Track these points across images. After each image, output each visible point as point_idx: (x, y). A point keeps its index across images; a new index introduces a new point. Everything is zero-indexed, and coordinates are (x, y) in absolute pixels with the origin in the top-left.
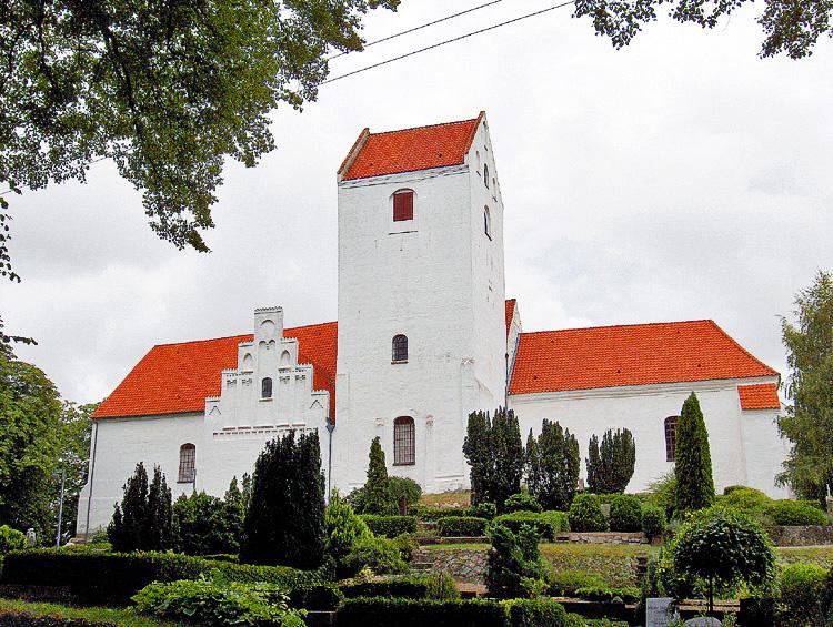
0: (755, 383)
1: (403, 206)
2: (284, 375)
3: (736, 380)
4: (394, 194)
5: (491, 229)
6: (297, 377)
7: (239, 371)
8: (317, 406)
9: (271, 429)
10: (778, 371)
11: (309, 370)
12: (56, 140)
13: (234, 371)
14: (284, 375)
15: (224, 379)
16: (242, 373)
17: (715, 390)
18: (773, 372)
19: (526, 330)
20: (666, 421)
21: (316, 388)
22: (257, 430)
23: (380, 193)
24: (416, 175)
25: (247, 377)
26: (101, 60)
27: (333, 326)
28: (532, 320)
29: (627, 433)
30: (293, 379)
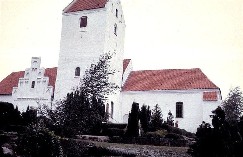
0: (208, 91)
1: (84, 22)
2: (39, 80)
3: (202, 90)
4: (81, 18)
5: (118, 32)
6: (43, 81)
7: (24, 78)
8: (48, 91)
9: (33, 99)
10: (219, 87)
11: (47, 79)
12: (111, 85)
13: (23, 78)
14: (39, 80)
15: (20, 81)
16: (26, 79)
17: (193, 93)
18: (217, 87)
19: (134, 70)
20: (177, 103)
21: (49, 85)
22: (29, 99)
23: (76, 17)
24: (88, 11)
25: (27, 81)
26: (85, 85)
27: (56, 68)
28: (136, 66)
29: (183, 118)
30: (41, 82)
